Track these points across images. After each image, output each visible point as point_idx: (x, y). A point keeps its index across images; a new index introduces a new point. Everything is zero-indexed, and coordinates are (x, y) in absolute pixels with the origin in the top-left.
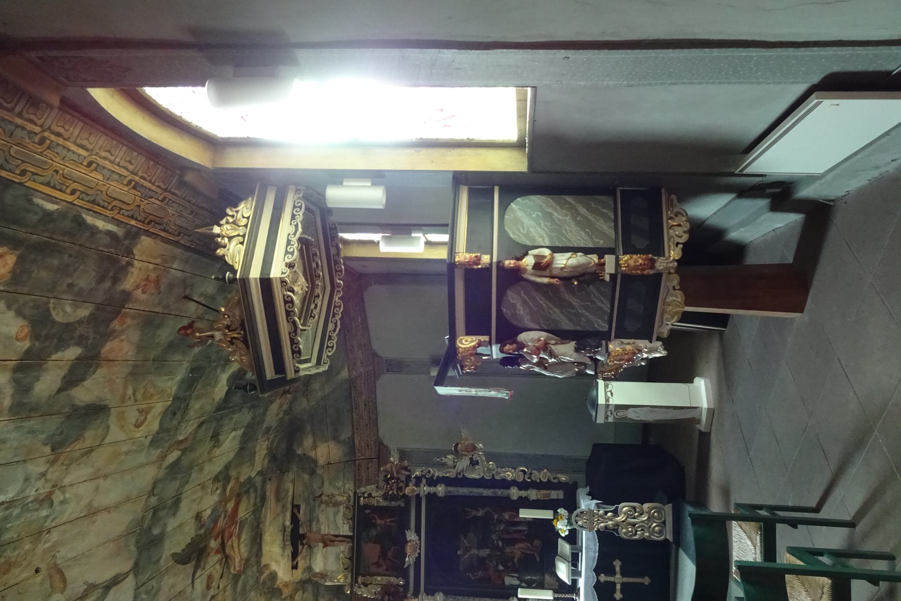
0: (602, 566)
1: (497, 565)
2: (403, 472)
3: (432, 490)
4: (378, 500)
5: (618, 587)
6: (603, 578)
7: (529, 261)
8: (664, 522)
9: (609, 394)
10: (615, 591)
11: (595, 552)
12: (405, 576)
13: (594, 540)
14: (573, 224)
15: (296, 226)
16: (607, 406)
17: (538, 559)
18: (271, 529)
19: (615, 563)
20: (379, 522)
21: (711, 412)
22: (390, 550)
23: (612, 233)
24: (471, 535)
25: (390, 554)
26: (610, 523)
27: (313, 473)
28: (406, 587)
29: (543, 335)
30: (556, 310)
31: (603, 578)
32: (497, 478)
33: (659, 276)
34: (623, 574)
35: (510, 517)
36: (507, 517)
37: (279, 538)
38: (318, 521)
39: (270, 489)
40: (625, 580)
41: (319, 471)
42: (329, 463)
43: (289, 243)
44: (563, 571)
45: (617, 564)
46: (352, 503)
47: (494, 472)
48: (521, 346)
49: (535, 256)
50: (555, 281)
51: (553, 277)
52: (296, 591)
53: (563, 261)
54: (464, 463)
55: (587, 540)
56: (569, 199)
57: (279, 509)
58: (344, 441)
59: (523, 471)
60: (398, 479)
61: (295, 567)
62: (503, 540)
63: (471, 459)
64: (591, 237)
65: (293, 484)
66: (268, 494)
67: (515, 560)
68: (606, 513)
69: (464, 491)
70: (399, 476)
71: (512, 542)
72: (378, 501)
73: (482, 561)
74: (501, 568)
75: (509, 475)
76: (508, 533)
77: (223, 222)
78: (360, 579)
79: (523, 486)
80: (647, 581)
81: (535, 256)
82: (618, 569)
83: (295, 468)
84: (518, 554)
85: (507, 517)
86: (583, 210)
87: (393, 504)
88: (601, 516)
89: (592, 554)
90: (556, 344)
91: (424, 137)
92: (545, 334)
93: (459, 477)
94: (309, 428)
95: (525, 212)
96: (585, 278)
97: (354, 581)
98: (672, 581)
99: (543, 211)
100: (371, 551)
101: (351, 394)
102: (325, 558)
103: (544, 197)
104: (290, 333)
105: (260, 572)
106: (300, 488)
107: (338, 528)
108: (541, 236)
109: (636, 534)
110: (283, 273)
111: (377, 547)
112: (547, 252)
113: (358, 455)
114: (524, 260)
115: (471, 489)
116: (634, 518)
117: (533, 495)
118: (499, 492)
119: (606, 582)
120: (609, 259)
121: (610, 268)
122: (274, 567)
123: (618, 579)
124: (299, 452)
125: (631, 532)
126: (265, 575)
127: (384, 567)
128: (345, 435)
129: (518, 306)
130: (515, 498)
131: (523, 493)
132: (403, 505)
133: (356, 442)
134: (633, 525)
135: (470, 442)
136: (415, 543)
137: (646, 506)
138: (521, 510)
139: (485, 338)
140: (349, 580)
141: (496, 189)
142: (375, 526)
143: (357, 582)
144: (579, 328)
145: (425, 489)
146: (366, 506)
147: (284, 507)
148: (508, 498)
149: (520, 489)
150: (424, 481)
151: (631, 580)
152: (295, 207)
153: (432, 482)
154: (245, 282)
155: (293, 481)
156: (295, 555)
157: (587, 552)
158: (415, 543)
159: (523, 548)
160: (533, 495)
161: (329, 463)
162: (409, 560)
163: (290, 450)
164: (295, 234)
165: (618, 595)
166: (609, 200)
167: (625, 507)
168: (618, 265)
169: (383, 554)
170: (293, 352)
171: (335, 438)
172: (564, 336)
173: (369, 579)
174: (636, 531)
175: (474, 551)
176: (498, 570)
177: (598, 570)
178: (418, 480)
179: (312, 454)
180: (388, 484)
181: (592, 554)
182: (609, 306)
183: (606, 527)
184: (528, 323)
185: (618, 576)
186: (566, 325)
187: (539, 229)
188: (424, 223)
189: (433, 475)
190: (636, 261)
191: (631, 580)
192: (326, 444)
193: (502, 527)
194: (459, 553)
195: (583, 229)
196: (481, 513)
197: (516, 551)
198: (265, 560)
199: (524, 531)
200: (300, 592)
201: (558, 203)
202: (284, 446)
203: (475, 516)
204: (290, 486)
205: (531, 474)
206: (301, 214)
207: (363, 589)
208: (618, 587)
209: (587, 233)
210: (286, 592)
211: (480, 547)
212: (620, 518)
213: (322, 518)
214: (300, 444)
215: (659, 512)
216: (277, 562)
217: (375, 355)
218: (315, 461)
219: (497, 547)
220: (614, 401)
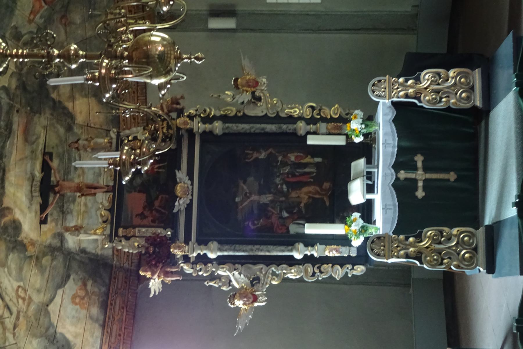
1: (281, 211)
3: (208, 126)
5: (420, 184)
6: (403, 175)
10: (416, 189)
11: (394, 147)
12: (175, 228)
13: (393, 135)
17: (328, 204)
18: (17, 170)
19: (416, 158)
22: (157, 198)
24: (251, 179)
25: (157, 203)
27: (69, 129)
31: (403, 175)
34: (426, 169)
35: (296, 157)
36: (293, 158)
37: (26, 187)
40: (428, 176)
41: (76, 130)
44: (356, 194)
45: (419, 159)
47: (279, 109)
52: (45, 255)
54: (247, 97)
55: (385, 134)
57: (28, 153)
61: (43, 222)
62: (287, 184)
63: (253, 93)
66: (15, 127)
67: (302, 205)
71: (297, 186)
73: (263, 209)
74: (285, 215)
75: (296, 112)
76: (294, 176)
78: (121, 231)
80: (452, 176)
82: (420, 164)
84: (305, 199)
85: (293, 158)
88: (401, 84)
89: (390, 149)
93: (239, 115)
98: (480, 183)
109: (440, 101)
110: (57, 342)
111: (143, 197)
116: (439, 84)
119: (406, 179)
122: (18, 215)
123: (420, 175)
125: (436, 98)
127: (150, 219)
134: (437, 92)
135: (253, 77)
136: (187, 189)
143: (116, 235)
151: (435, 176)
155: (45, 128)
156: (43, 207)
157: (385, 147)
158: (187, 189)
159: (310, 192)
162: (180, 204)
165: (420, 194)
169: (149, 204)
174: (441, 98)
175: (254, 197)
176: (281, 217)
177: (397, 166)
179: (69, 105)
181: (390, 149)
185: (420, 172)
189: (209, 115)
191: (435, 176)
192: (85, 100)
193: (287, 169)
194: (237, 200)
196: (263, 155)
197: (302, 195)
199: (313, 173)
200: (48, 258)
203: (257, 158)
205: (320, 110)
208: (420, 184)
210: (31, 251)
212: (425, 84)
215: (466, 78)
216: (22, 211)
218: (71, 116)
219: (281, 192)
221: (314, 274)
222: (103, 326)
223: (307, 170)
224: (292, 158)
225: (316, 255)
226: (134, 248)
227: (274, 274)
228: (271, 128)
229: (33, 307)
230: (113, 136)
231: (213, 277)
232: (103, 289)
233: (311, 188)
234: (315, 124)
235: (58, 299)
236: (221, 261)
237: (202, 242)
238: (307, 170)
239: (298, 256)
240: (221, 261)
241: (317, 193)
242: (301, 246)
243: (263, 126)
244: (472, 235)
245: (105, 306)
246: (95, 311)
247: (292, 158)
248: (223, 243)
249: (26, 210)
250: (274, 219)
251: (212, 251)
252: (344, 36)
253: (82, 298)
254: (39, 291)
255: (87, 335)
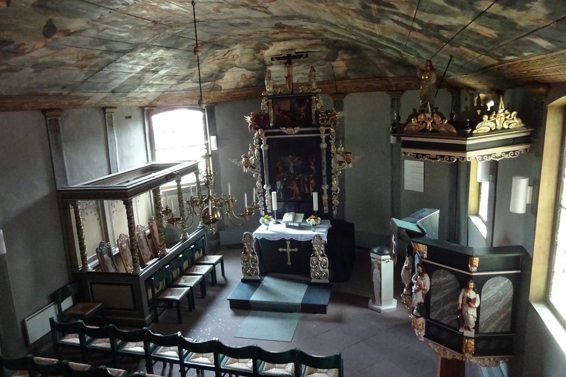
0: (294, 242)
1: (286, 177)
2: (333, 123)
3: (324, 141)
4: (316, 107)
5: (285, 250)
6: (288, 243)
7: (472, 294)
8: (319, 278)
9: (387, 261)
10: (282, 248)
12: (275, 127)
14: (494, 312)
15: (501, 157)
16: (380, 260)
20: (303, 108)
21: (379, 311)
23: (487, 331)
24: (300, 162)
25: (286, 116)
26: (317, 252)
27: (327, 60)
28: (269, 128)
29: (427, 287)
30: (442, 297)
31: (288, 243)
32: (333, 176)
33: (462, 353)
34: (291, 252)
38: (298, 66)
39: (318, 41)
40: (289, 254)
41: (328, 63)
42: (333, 67)
43: (489, 155)
45: (296, 250)
46: (312, 92)
48: (421, 275)
49: (475, 299)
50: (460, 306)
51: (462, 305)
52: (259, 60)
53: (472, 313)
54: (340, 158)
56: (510, 309)
58: (347, 74)
59: (337, 191)
60: (328, 119)
63: (342, 162)
64: (486, 321)
65: (320, 51)
68: (322, 251)
69: (324, 159)
70: (330, 121)
71: (299, 185)
72: (314, 108)
73: (286, 169)
74: (285, 179)
75: (335, 183)
76: (303, 182)
77: (507, 112)
78: (270, 101)
79: (329, 191)
80: (289, 263)
81: (475, 299)
82: (293, 250)
83: (329, 51)
86: (502, 317)
87: (314, 117)
88: (320, 249)
90: (423, 294)
91: (558, 247)
92: (428, 289)
94: (355, 56)
95: (503, 287)
96: (462, 321)
97: (269, 98)
99: (503, 296)
100: (286, 105)
101: (377, 78)
102: (278, 71)
103: (511, 296)
104: (429, 155)
105: (268, 43)
106: (317, 54)
107: (295, 75)
108: (487, 296)
112: (477, 305)
113: (339, 82)
114: (473, 291)
115: (325, 162)
117: (325, 197)
118: (325, 179)
119: (286, 244)
120: (472, 334)
121: (466, 333)
122: (271, 48)
123: (289, 250)
124: (340, 53)
126: (267, 45)
128: (351, 75)
129: (445, 278)
130: (323, 188)
131: (325, 192)
132: (313, 123)
133: (347, 81)
134: (317, 264)
136: (292, 132)
137: (327, 270)
138: (317, 193)
139: (425, 256)
140: (269, 94)
141: (519, 271)
142: (300, 106)
143: (269, 99)
144: (431, 304)
145: (323, 136)
146: (311, 100)
147: (306, 48)
148: (322, 184)
149: (327, 190)
150: (328, 134)
152: (514, 152)
153: (328, 139)
154: (466, 136)
155: (321, 51)
156: (279, 58)
158: (292, 132)
160: (325, 197)
161: (333, 67)
162: (284, 130)
163: (341, 48)
164: (496, 157)
165: (281, 250)
166: (508, 328)
167: (326, 260)
168: (469, 338)
169: (285, 112)
170: (417, 154)
171: (349, 70)
172: (427, 297)
173: (271, 106)
175: (292, 164)
178: (328, 131)
179: (339, 59)
180: (325, 113)
182: (445, 323)
183: (315, 251)
184: (434, 281)
186: (433, 299)
187: (491, 296)
188: (498, 185)
190: (470, 348)
191: (289, 256)
193: (306, 179)
195: (490, 317)
196: (312, 167)
198: (275, 44)
200: (258, 62)
201: (508, 303)
202: (343, 45)
204: (319, 49)
206: (510, 157)
207: (265, 103)
208: (285, 250)
209: (488, 319)
210: (258, 55)
211: (294, 167)
212: (321, 258)
213: (300, 68)
214: (345, 53)
215: (324, 276)
216: (274, 49)
217: (403, 91)
218: (334, 60)
220: (383, 264)
221: (259, 193)
222: (236, 88)
223: (306, 189)
224: (312, 182)
225: (266, 195)
226: (263, 108)
227: (258, 175)
228: (324, 172)
229: (231, 62)
230: (317, 91)
231: (253, 147)
232: (254, 85)
233: (298, 190)
234: (328, 193)
235: (240, 69)
236: (260, 150)
237: (268, 142)
238: (306, 189)
239: (265, 187)
240: (260, 150)
241: (296, 194)
242: (269, 188)
243: (325, 169)
244: (256, 274)
245: (246, 87)
246: (242, 84)
247: (312, 182)
248: (268, 152)
249: (277, 50)
250: (282, 174)
251: (264, 147)
252: (389, 199)
253: (245, 78)
254: (240, 62)
255: (229, 84)
